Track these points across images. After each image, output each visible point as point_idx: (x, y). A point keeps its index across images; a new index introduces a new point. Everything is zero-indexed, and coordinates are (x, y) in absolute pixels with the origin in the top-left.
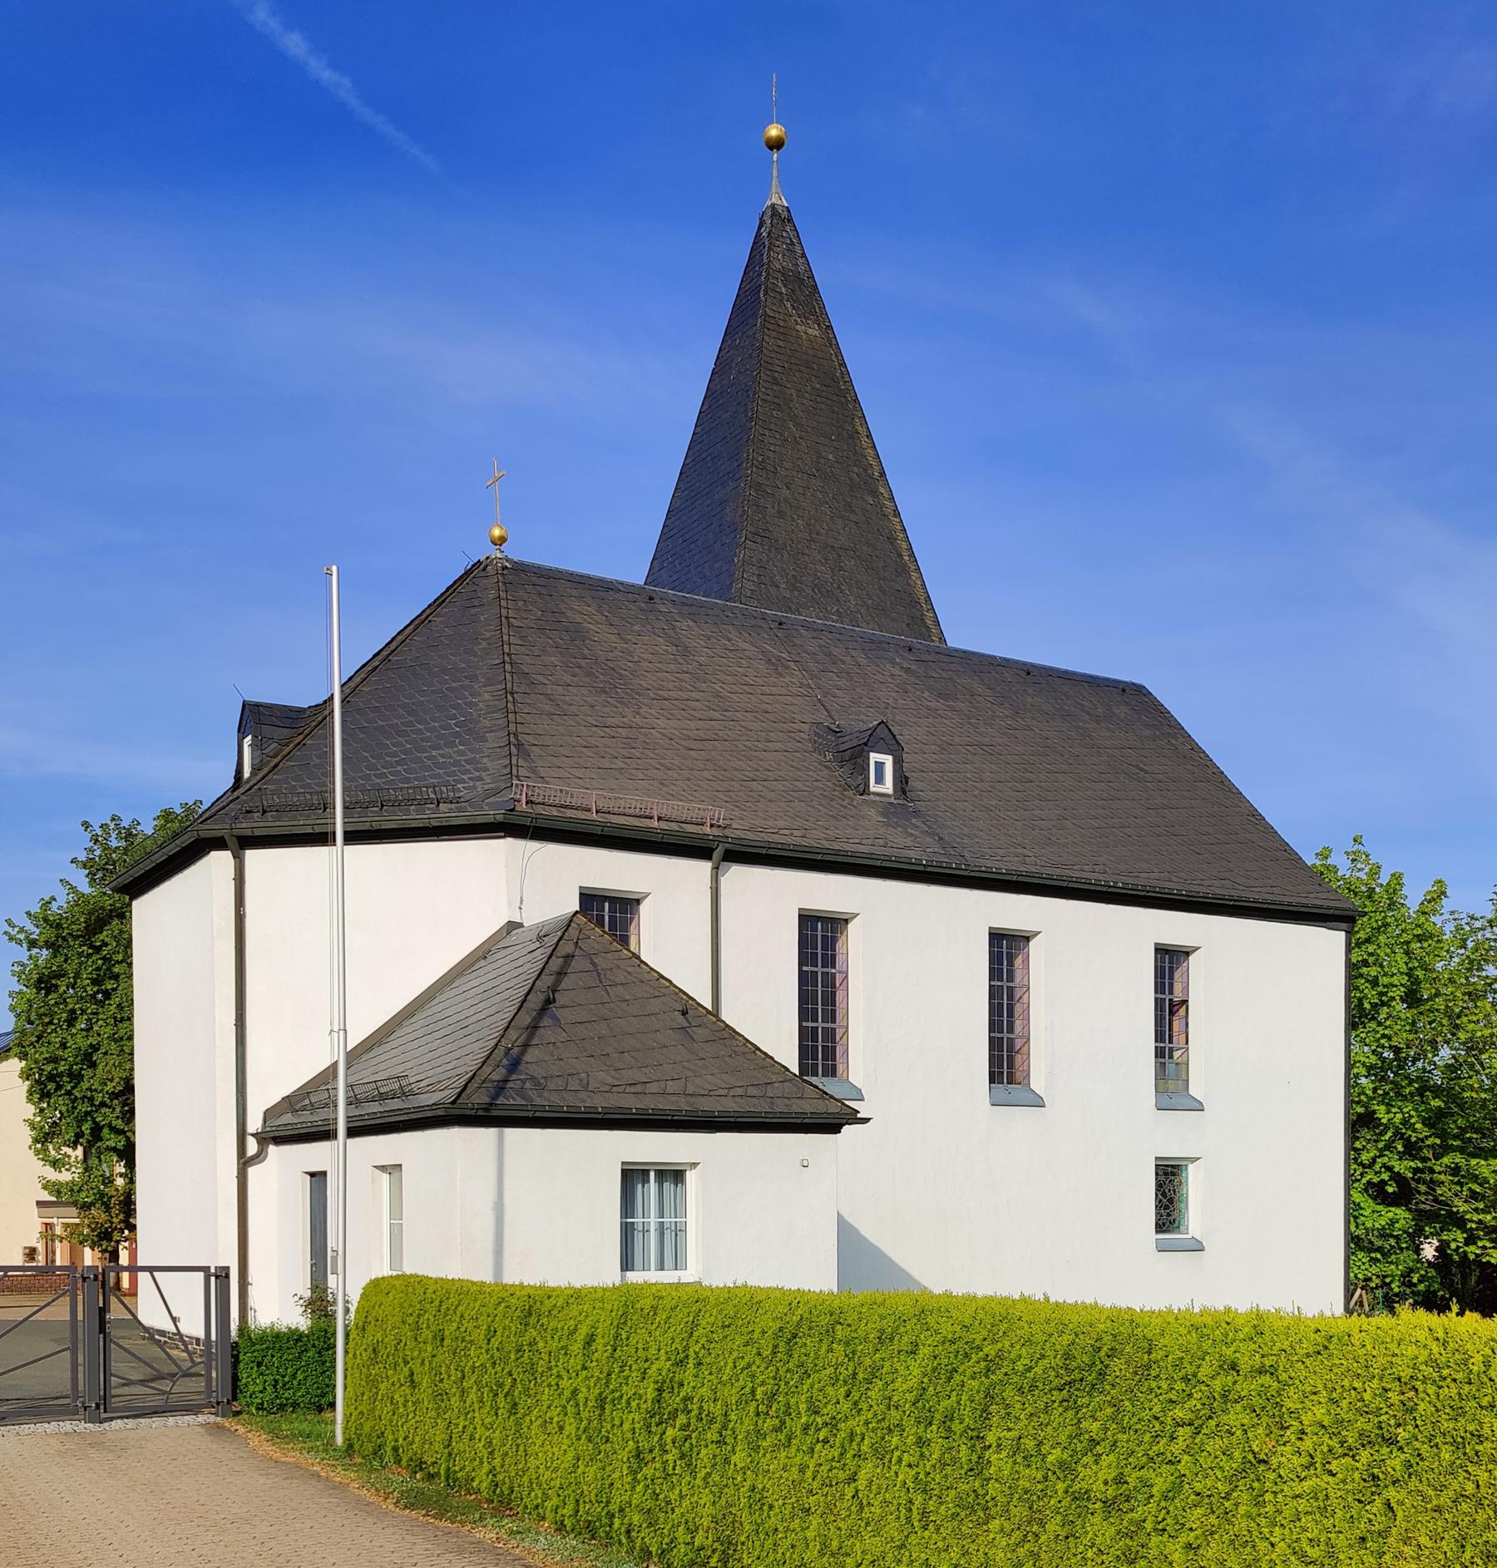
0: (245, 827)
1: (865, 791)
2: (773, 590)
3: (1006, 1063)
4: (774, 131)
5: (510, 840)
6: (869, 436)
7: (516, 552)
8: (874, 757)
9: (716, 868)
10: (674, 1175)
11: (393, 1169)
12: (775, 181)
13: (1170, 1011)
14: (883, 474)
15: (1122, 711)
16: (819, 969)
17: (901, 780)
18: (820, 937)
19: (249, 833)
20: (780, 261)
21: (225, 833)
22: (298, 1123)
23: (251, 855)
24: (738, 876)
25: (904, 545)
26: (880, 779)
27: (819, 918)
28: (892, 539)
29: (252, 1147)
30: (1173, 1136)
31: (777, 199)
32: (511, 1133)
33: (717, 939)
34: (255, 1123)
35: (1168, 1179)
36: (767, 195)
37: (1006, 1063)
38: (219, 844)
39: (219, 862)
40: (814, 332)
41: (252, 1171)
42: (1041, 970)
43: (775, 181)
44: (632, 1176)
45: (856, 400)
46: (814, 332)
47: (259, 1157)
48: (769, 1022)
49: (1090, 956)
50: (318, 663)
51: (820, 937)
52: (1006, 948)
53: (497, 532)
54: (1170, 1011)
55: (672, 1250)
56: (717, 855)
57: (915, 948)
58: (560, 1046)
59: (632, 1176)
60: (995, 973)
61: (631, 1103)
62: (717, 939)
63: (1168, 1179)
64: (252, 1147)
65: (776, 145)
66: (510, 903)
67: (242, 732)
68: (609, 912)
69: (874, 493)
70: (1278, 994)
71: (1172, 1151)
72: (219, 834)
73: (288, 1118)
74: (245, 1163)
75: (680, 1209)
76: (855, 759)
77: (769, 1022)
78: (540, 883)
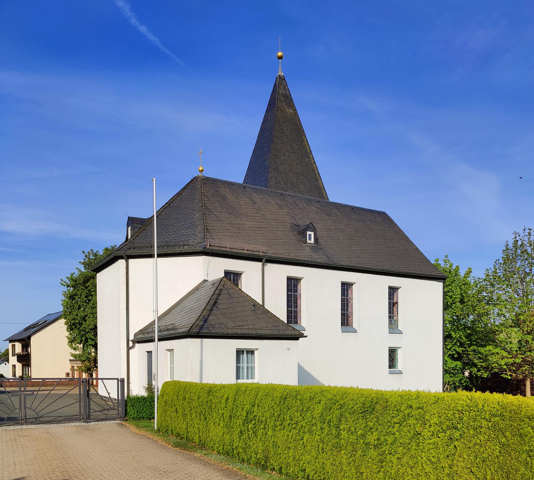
0: (129, 253)
1: (306, 242)
2: (279, 185)
3: (346, 320)
4: (280, 54)
5: (204, 256)
6: (307, 141)
7: (206, 174)
8: (308, 233)
9: (263, 264)
10: (251, 352)
11: (171, 350)
12: (280, 68)
13: (393, 305)
14: (311, 152)
15: (379, 219)
16: (293, 293)
17: (316, 239)
18: (293, 284)
19: (130, 254)
20: (281, 91)
21: (123, 255)
22: (144, 337)
23: (131, 261)
24: (270, 267)
25: (317, 172)
26: (310, 239)
27: (232, 273)
28: (313, 170)
29: (131, 344)
30: (394, 341)
31: (281, 73)
32: (205, 340)
33: (264, 285)
34: (132, 337)
35: (392, 353)
36: (278, 72)
37: (346, 320)
38: (121, 257)
39: (121, 263)
40: (291, 111)
41: (131, 351)
42: (356, 293)
43: (280, 68)
44: (239, 352)
45: (303, 131)
46: (291, 111)
47: (133, 347)
48: (279, 310)
49: (370, 290)
50: (150, 206)
51: (293, 284)
52: (346, 287)
53: (201, 168)
54: (393, 305)
55: (251, 374)
56: (263, 260)
57: (320, 287)
58: (219, 315)
59: (239, 352)
60: (343, 294)
61: (239, 331)
62: (264, 285)
63: (392, 353)
64: (131, 344)
65: (280, 58)
66: (204, 274)
67: (128, 225)
68: (233, 277)
69: (308, 157)
70: (424, 301)
71: (393, 345)
72: (121, 255)
73: (141, 336)
74: (129, 349)
75: (253, 362)
76: (303, 233)
77: (279, 310)
78: (213, 268)
